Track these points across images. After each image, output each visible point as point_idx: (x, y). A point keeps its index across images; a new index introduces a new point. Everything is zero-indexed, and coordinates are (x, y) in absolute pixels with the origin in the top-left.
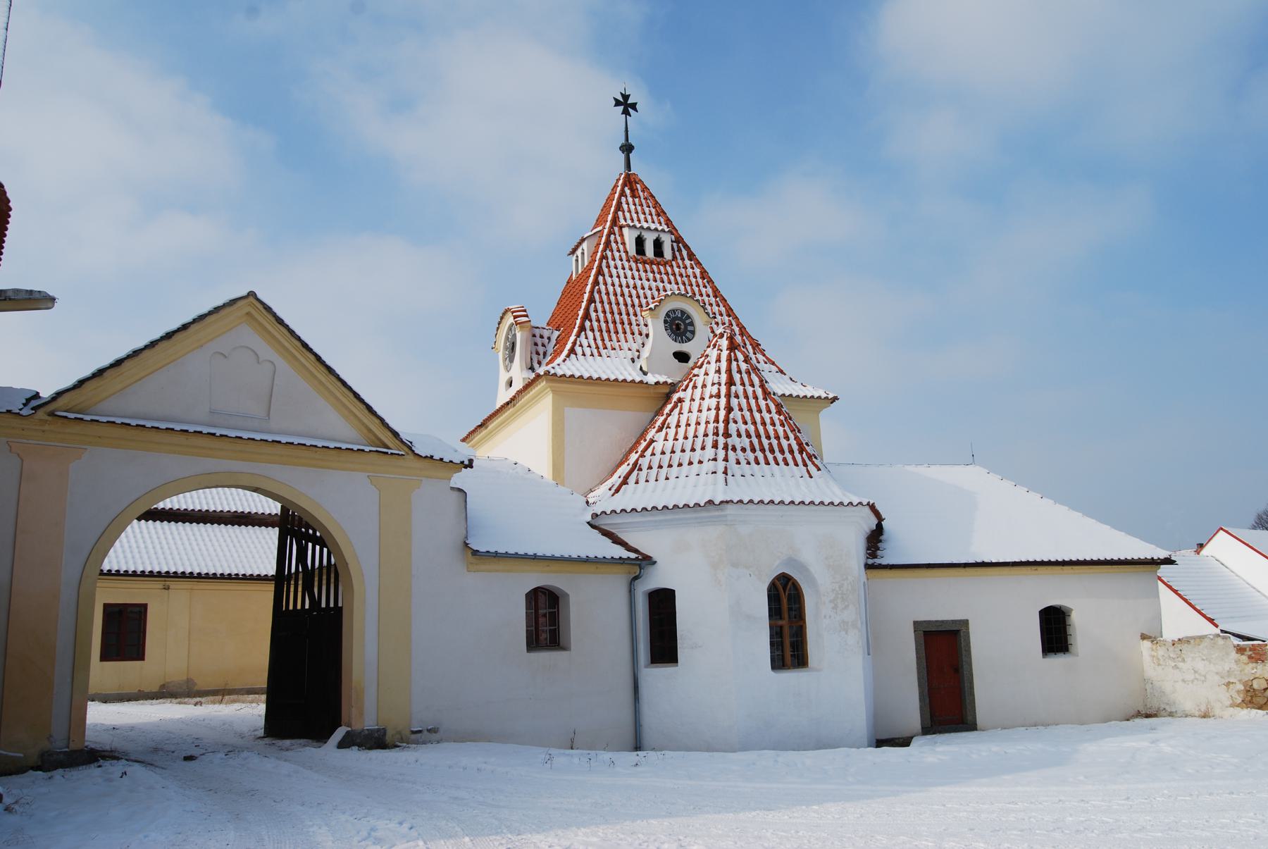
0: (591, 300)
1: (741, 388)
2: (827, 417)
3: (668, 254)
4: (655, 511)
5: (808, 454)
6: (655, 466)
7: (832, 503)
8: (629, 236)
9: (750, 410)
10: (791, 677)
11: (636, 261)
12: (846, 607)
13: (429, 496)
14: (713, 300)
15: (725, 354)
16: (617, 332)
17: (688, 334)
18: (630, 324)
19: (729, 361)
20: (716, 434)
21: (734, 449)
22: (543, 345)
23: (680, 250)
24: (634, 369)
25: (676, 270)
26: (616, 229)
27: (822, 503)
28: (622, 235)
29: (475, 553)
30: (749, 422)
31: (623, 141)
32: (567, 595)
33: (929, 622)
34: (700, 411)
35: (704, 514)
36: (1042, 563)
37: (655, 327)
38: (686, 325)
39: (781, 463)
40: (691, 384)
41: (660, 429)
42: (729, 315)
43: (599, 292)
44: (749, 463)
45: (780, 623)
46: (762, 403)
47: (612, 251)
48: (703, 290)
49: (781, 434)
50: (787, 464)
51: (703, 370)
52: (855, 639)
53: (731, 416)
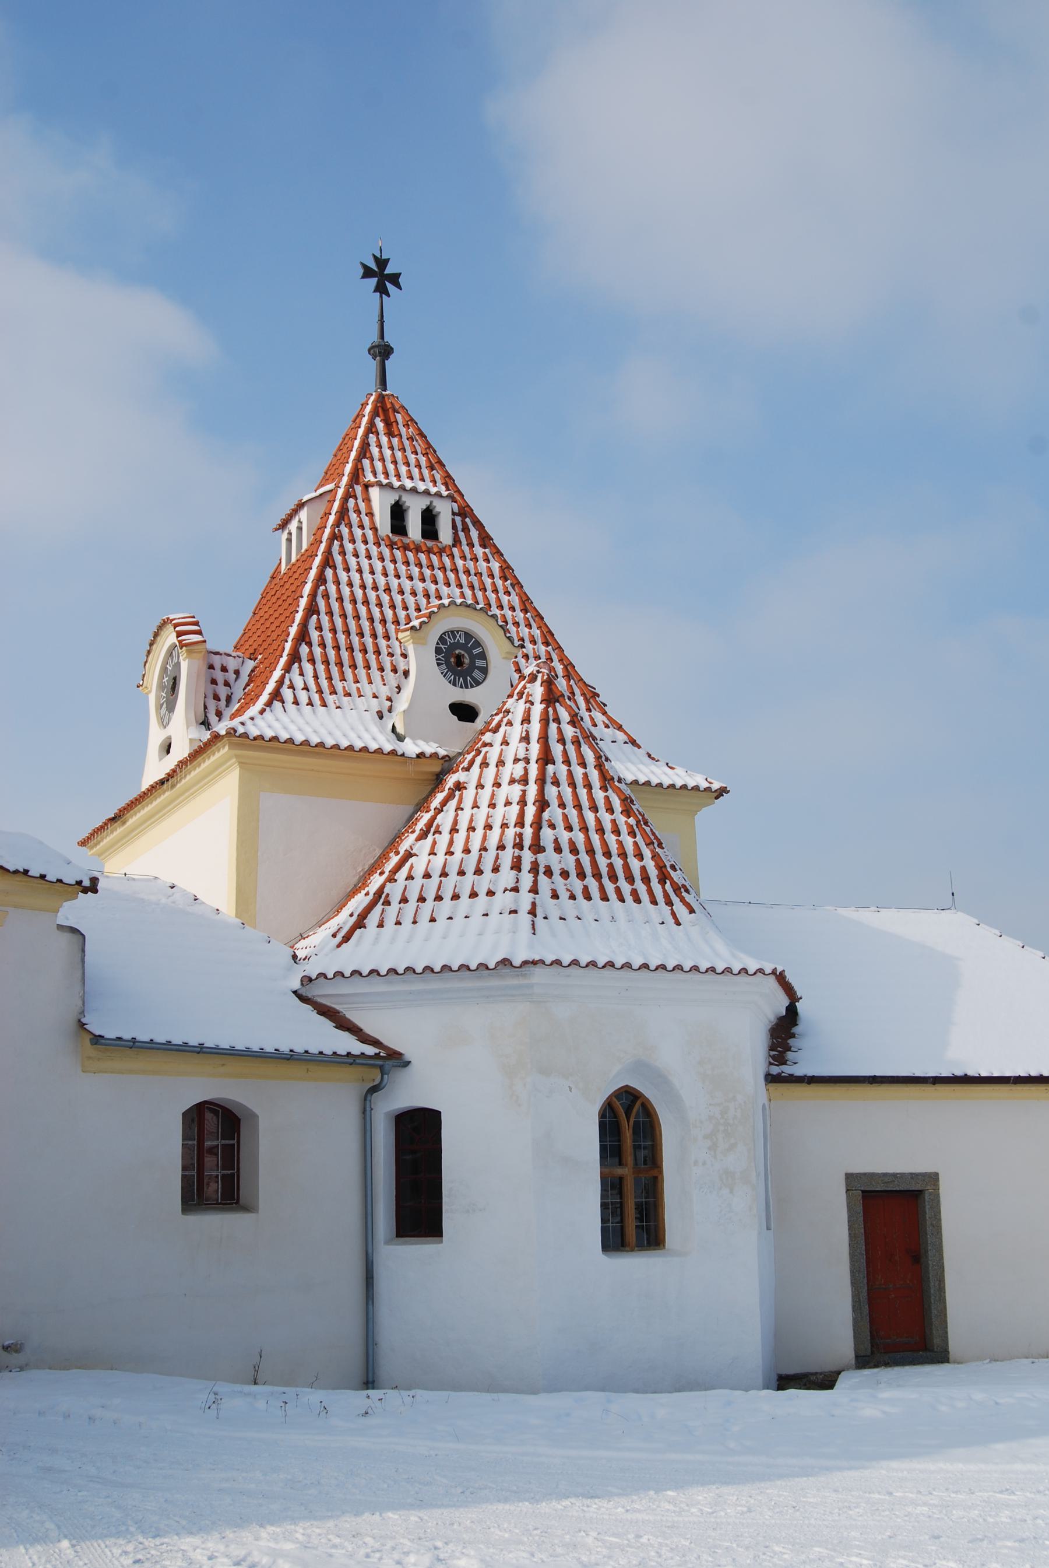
0: (312, 609)
3: (445, 536)
6: (413, 897)
7: (712, 969)
8: (380, 502)
10: (635, 1265)
11: (391, 545)
14: (520, 616)
15: (538, 709)
17: (476, 674)
18: (378, 652)
19: (545, 721)
20: (519, 845)
21: (549, 872)
22: (227, 684)
23: (466, 529)
24: (382, 730)
25: (460, 563)
26: (358, 489)
28: (367, 500)
29: (97, 1039)
30: (576, 826)
31: (374, 338)
33: (871, 1176)
35: (494, 982)
38: (473, 658)
39: (629, 898)
40: (479, 760)
41: (423, 835)
42: (547, 644)
43: (326, 596)
45: (619, 1171)
46: (599, 795)
47: (350, 526)
48: (505, 599)
50: (638, 900)
51: (499, 736)
53: (546, 815)
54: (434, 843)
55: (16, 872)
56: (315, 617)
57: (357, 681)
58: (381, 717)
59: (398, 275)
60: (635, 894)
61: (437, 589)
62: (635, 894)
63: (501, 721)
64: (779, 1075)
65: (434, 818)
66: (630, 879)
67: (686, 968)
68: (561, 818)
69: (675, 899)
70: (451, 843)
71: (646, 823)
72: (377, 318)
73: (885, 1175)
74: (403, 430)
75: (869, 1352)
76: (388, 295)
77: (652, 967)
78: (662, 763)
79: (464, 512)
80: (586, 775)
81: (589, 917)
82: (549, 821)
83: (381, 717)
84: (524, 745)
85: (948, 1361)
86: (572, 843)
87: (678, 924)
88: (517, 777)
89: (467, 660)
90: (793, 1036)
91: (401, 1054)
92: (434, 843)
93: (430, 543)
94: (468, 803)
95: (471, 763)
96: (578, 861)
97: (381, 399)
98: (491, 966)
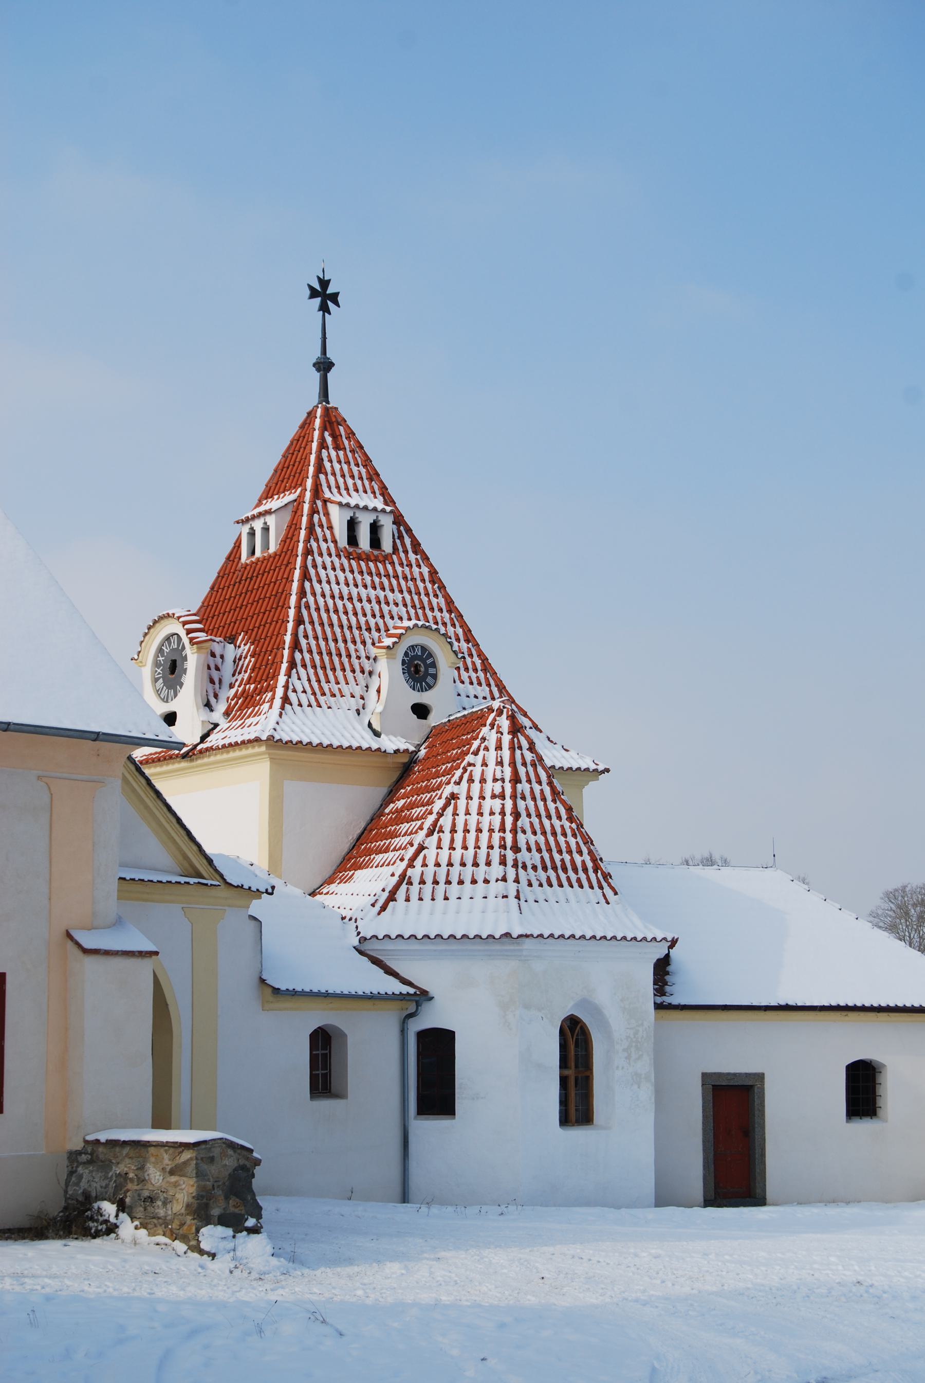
0: (299, 621)
1: (528, 786)
2: (592, 792)
3: (387, 545)
4: (439, 940)
5: (603, 873)
6: (429, 879)
7: (635, 939)
9: (539, 816)
10: (577, 1134)
12: (639, 1058)
13: (231, 923)
14: (446, 615)
15: (506, 738)
16: (334, 669)
18: (349, 656)
19: (512, 749)
20: (503, 847)
21: (525, 867)
22: (217, 669)
23: (401, 537)
24: (361, 723)
25: (399, 569)
27: (624, 938)
28: (327, 514)
29: (276, 991)
30: (539, 832)
31: (318, 353)
32: (346, 1036)
33: (719, 1075)
34: (480, 814)
35: (497, 947)
36: (855, 1009)
37: (388, 672)
39: (575, 885)
40: (466, 776)
41: (430, 833)
42: (467, 641)
43: (308, 607)
44: (541, 885)
46: (552, 806)
47: (317, 540)
48: (434, 601)
49: (574, 847)
50: (581, 886)
51: (479, 759)
52: (646, 1093)
53: (519, 823)
54: (440, 840)
55: (238, 886)
56: (302, 626)
57: (338, 683)
58: (359, 714)
59: (337, 294)
60: (579, 880)
61: (385, 596)
62: (579, 880)
63: (480, 746)
64: (662, 1003)
65: (437, 820)
66: (575, 870)
67: (619, 938)
68: (529, 825)
69: (604, 884)
70: (452, 841)
71: (582, 827)
72: (320, 335)
73: (729, 1074)
74: (346, 442)
75: (713, 1198)
76: (330, 313)
77: (598, 938)
78: (558, 747)
79: (399, 520)
80: (542, 790)
81: (552, 900)
82: (522, 828)
83: (359, 714)
84: (499, 768)
85: (760, 1201)
86: (537, 843)
87: (608, 903)
88: (497, 793)
89: (422, 669)
90: (668, 973)
91: (427, 992)
92: (440, 840)
93: (376, 553)
94: (461, 810)
95: (461, 778)
96: (542, 858)
97: (327, 412)
98: (497, 936)
